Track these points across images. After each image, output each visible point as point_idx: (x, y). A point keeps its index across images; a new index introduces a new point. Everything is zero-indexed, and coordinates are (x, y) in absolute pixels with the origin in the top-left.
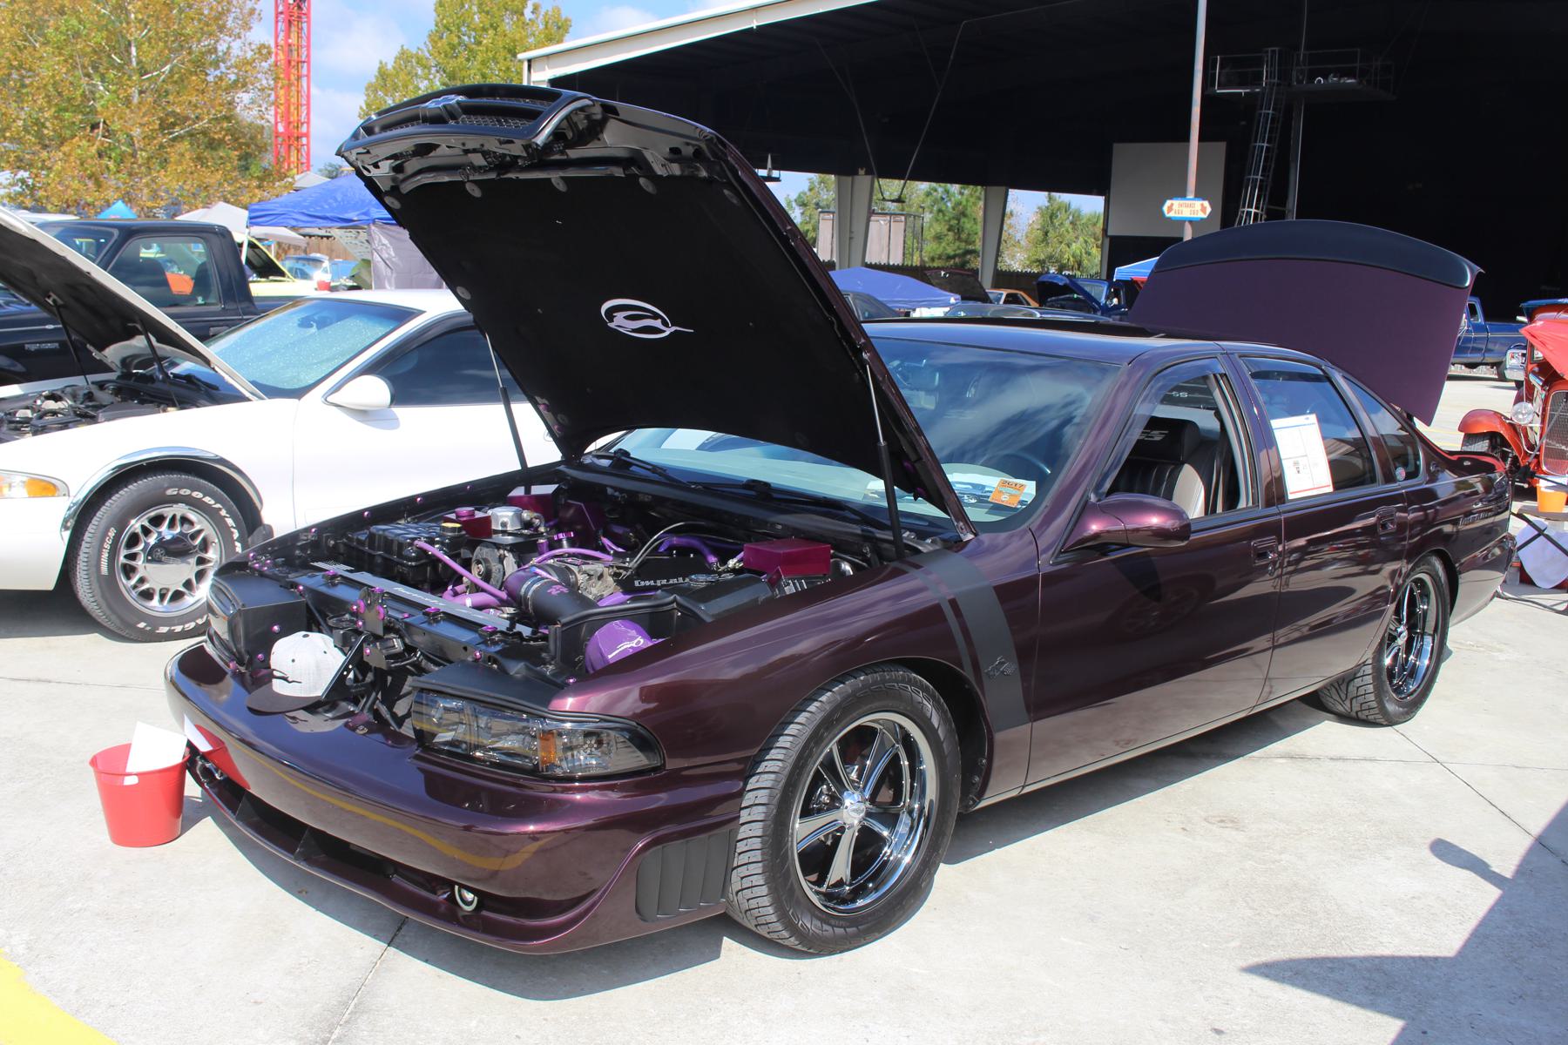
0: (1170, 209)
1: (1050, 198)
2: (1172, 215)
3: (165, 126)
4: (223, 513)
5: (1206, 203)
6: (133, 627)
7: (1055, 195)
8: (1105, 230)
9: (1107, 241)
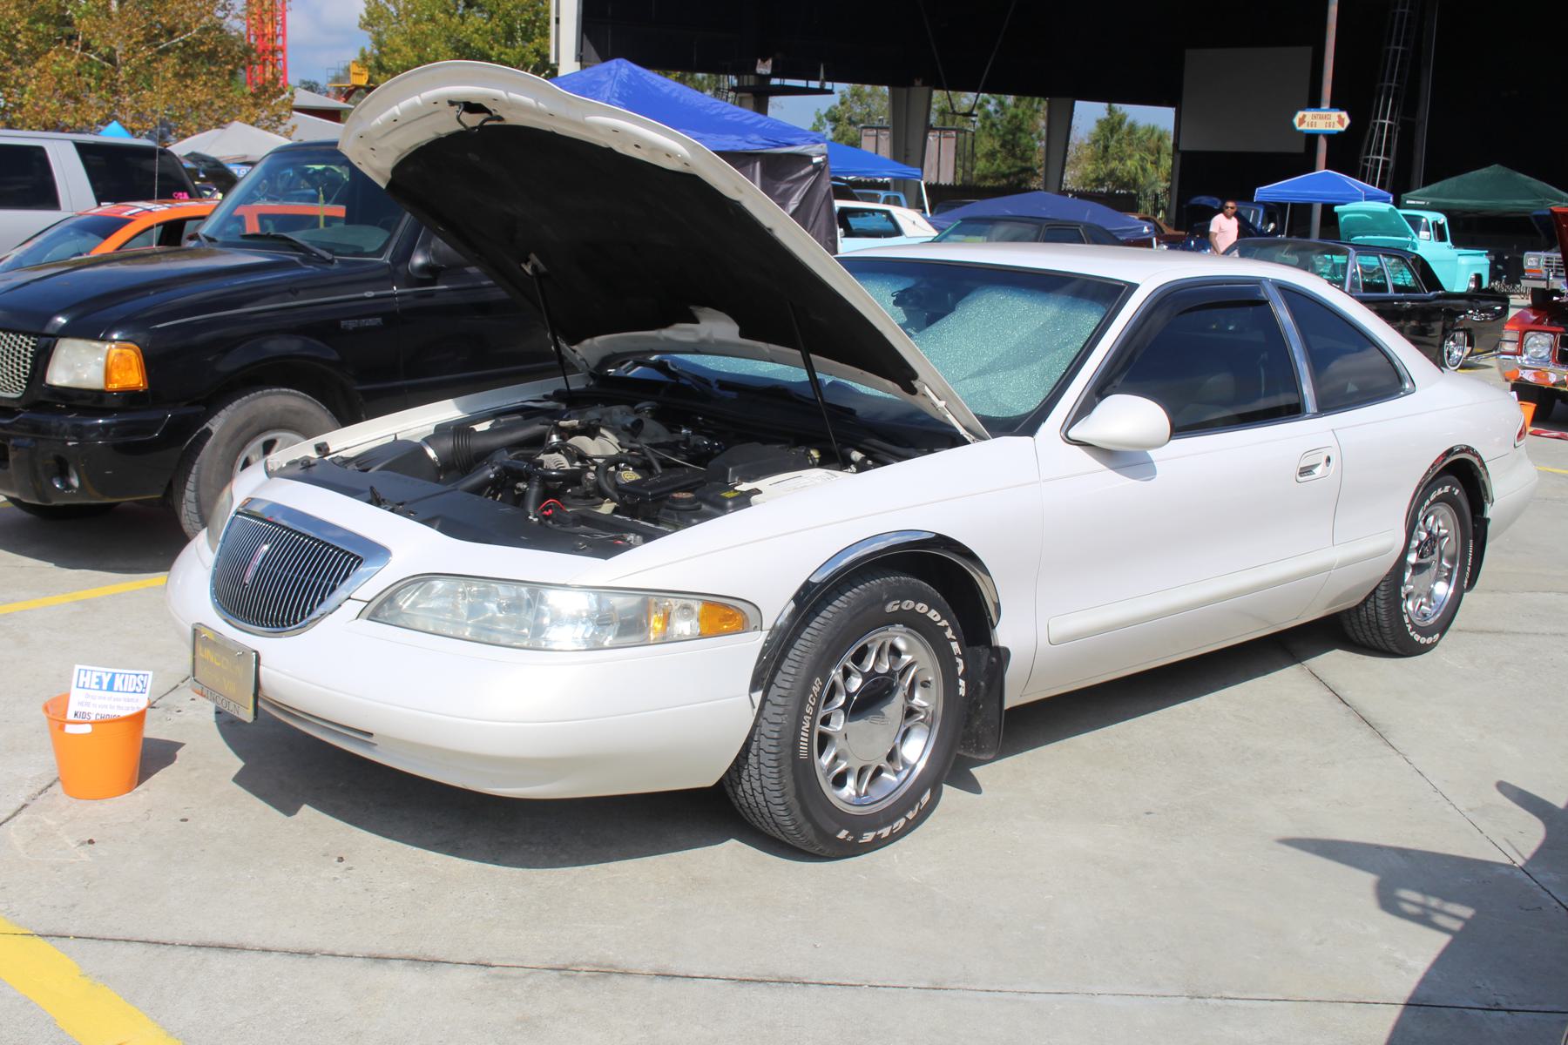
0: (1302, 121)
1: (1110, 110)
2: (1304, 127)
3: (151, 39)
4: (949, 634)
5: (1344, 115)
6: (830, 838)
7: (1116, 106)
8: (1176, 145)
9: (1178, 157)
